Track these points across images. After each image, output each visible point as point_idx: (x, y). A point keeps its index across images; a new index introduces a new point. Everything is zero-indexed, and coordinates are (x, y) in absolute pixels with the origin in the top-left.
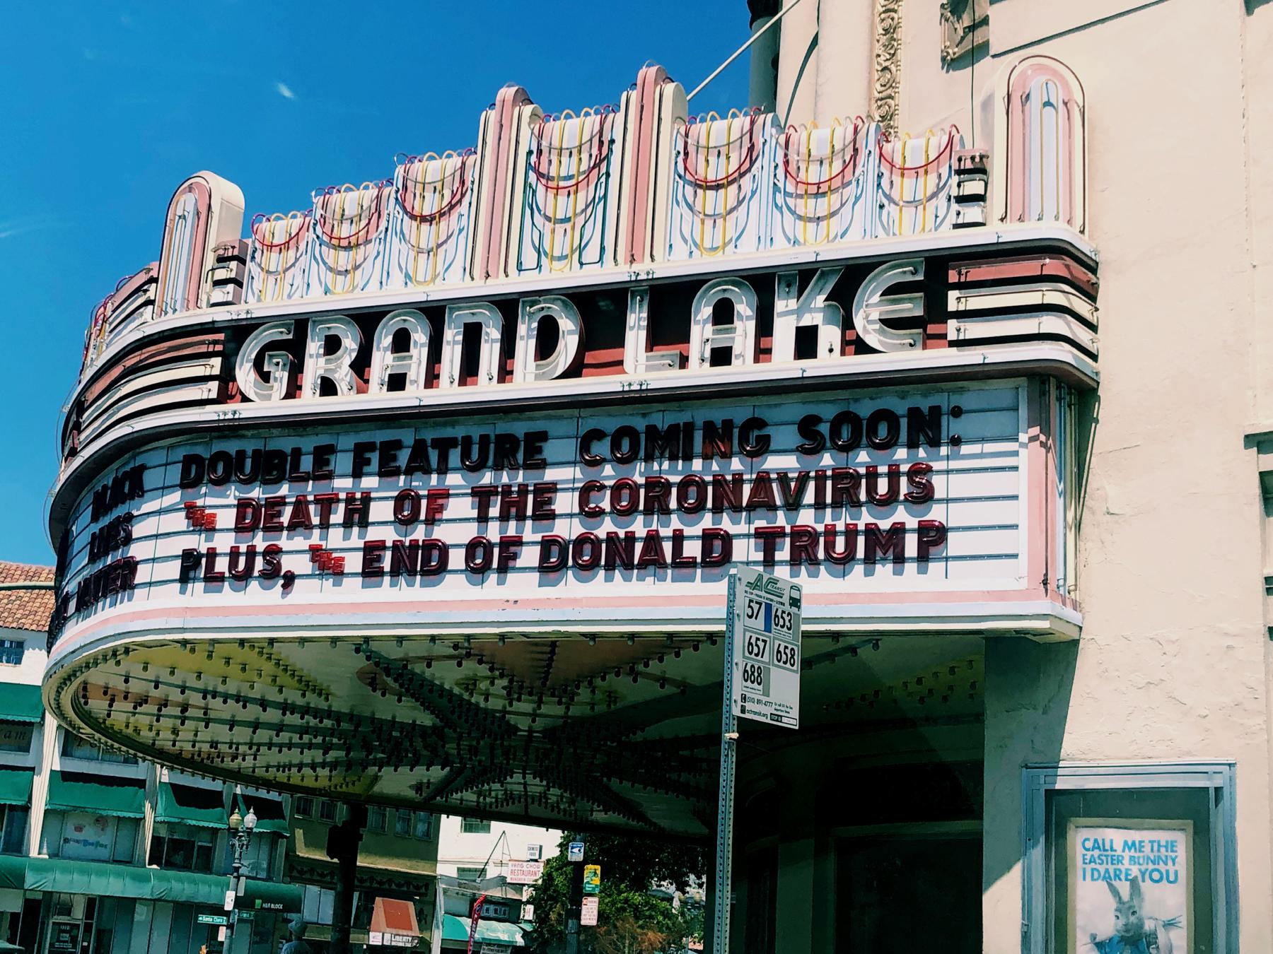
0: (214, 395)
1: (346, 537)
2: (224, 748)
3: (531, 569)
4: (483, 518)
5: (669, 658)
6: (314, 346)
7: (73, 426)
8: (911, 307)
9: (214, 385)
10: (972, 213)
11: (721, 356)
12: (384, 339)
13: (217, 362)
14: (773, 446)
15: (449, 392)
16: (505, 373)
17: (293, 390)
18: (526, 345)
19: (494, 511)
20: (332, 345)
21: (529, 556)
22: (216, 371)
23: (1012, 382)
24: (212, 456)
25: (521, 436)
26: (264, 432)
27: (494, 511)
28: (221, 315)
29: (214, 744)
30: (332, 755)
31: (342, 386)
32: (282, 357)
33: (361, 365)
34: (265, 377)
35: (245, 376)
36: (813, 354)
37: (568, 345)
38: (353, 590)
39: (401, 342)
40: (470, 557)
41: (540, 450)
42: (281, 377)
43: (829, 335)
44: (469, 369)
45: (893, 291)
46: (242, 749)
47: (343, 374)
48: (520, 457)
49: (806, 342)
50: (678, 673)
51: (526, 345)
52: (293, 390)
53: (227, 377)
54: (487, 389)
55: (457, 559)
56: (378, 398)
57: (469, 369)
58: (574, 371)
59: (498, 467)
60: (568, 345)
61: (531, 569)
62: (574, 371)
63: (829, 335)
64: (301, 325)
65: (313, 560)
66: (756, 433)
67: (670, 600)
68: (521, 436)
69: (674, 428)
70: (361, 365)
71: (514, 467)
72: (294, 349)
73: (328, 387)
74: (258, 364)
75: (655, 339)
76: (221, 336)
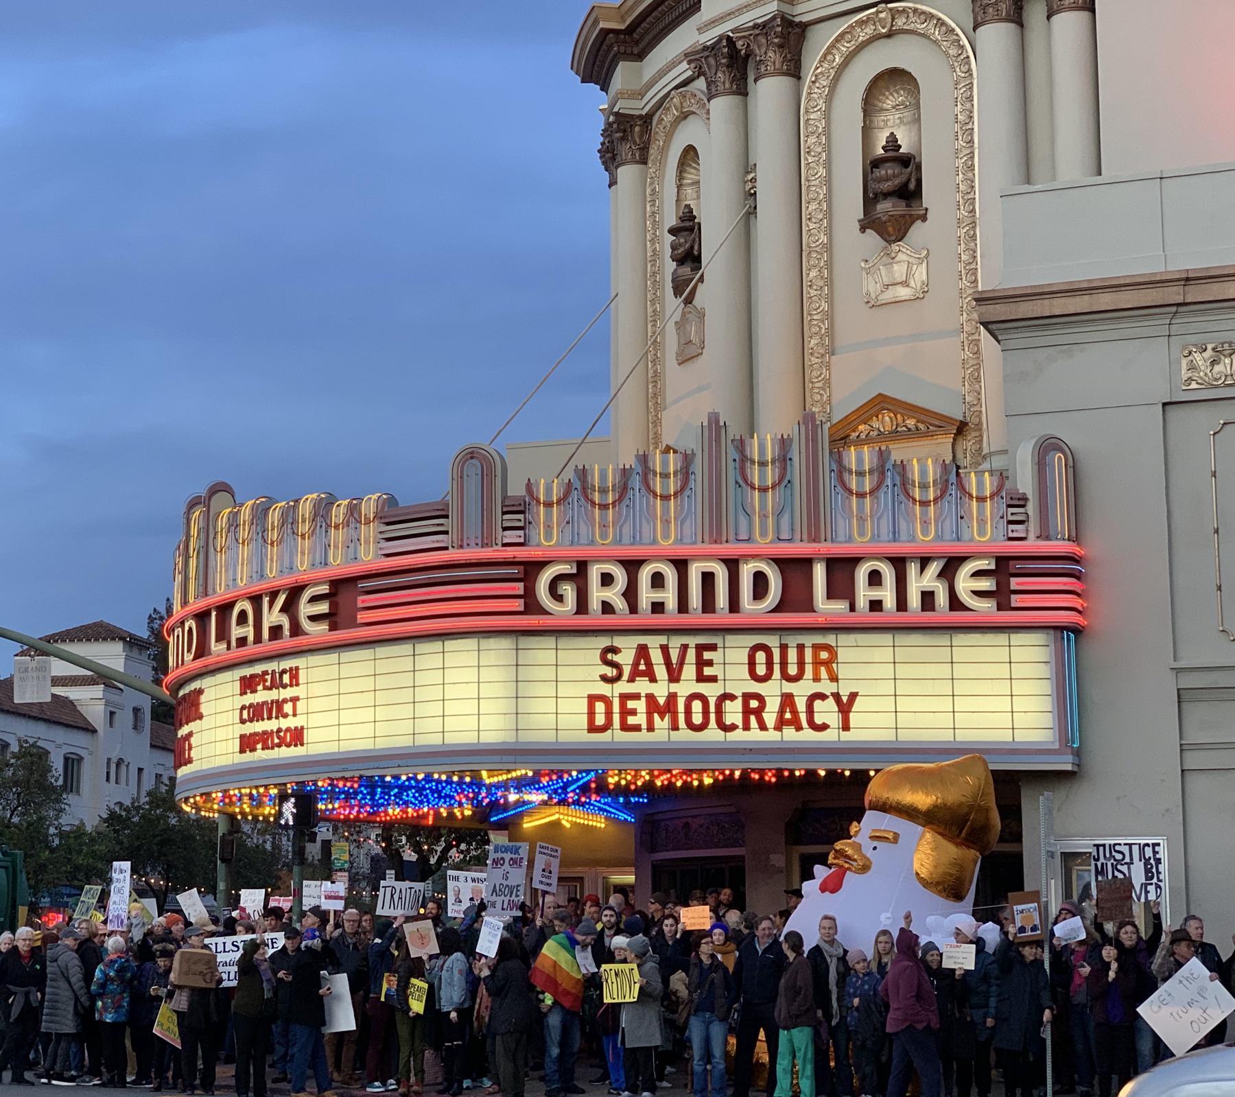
8: (986, 584)
10: (1019, 530)
33: (630, 594)
34: (559, 598)
43: (942, 599)
45: (978, 574)
47: (620, 604)
49: (928, 598)
52: (582, 606)
63: (942, 599)
70: (630, 594)
72: (580, 576)
75: (831, 595)
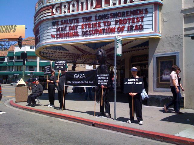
0: (51, 14)
1: (88, 29)
2: (58, 58)
3: (126, 31)
4: (105, 26)
5: (110, 44)
6: (63, 7)
7: (35, 20)
9: (51, 13)
11: (73, 11)
12: (71, 6)
13: (51, 10)
14: (149, 12)
15: (80, 11)
16: (87, 9)
17: (61, 13)
18: (89, 5)
19: (87, 27)
20: (65, 6)
21: (126, 29)
22: (51, 11)
23: (152, 5)
24: (55, 22)
25: (125, 12)
26: (131, 8)
27: (87, 27)
28: (51, 4)
29: (57, 58)
30: (70, 59)
31: (66, 12)
32: (59, 9)
33: (69, 9)
35: (54, 11)
36: (121, 4)
37: (95, 5)
38: (55, 40)
39: (73, 5)
40: (118, 29)
41: (91, 19)
42: (59, 12)
44: (82, 9)
46: (60, 58)
47: (66, 10)
48: (125, 15)
49: (65, 12)
50: (109, 46)
51: (89, 5)
52: (61, 13)
53: (52, 12)
54: (85, 11)
55: (116, 30)
56: (71, 13)
57: (82, 9)
58: (95, 8)
59: (122, 17)
60: (95, 5)
61: (126, 31)
62: (95, 8)
64: (61, 4)
65: (51, 36)
66: (108, 16)
67: (139, 34)
68: (125, 12)
69: (134, 11)
71: (125, 16)
72: (60, 7)
73: (65, 12)
74: (56, 9)
76: (51, 7)
